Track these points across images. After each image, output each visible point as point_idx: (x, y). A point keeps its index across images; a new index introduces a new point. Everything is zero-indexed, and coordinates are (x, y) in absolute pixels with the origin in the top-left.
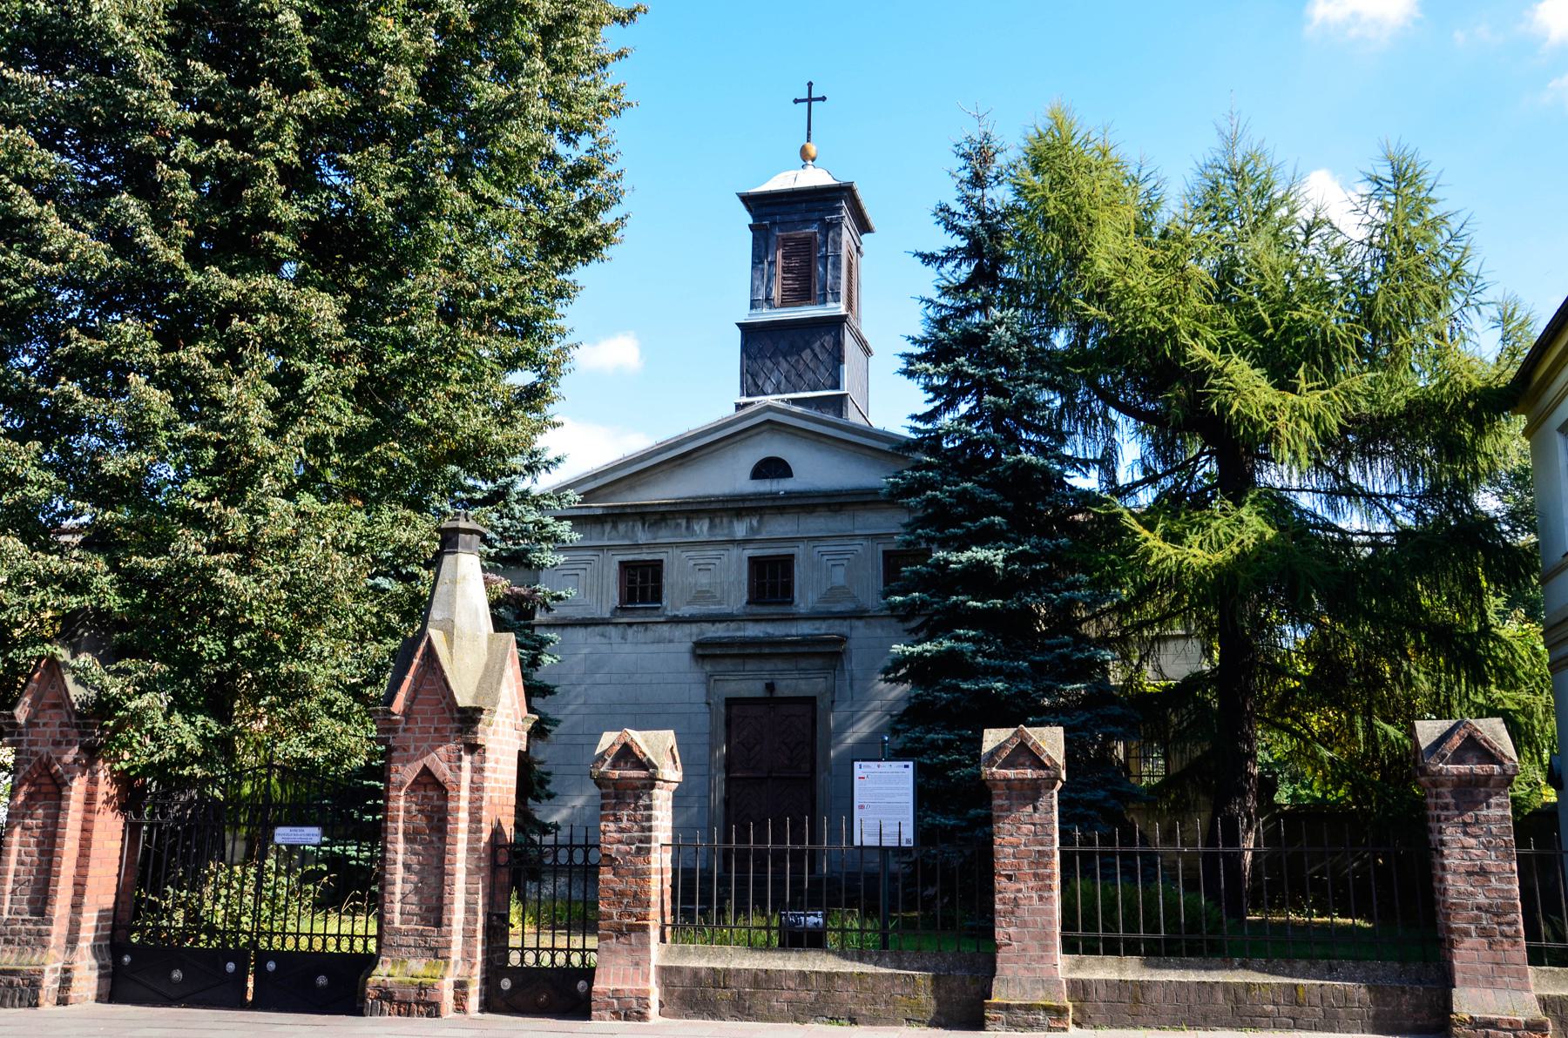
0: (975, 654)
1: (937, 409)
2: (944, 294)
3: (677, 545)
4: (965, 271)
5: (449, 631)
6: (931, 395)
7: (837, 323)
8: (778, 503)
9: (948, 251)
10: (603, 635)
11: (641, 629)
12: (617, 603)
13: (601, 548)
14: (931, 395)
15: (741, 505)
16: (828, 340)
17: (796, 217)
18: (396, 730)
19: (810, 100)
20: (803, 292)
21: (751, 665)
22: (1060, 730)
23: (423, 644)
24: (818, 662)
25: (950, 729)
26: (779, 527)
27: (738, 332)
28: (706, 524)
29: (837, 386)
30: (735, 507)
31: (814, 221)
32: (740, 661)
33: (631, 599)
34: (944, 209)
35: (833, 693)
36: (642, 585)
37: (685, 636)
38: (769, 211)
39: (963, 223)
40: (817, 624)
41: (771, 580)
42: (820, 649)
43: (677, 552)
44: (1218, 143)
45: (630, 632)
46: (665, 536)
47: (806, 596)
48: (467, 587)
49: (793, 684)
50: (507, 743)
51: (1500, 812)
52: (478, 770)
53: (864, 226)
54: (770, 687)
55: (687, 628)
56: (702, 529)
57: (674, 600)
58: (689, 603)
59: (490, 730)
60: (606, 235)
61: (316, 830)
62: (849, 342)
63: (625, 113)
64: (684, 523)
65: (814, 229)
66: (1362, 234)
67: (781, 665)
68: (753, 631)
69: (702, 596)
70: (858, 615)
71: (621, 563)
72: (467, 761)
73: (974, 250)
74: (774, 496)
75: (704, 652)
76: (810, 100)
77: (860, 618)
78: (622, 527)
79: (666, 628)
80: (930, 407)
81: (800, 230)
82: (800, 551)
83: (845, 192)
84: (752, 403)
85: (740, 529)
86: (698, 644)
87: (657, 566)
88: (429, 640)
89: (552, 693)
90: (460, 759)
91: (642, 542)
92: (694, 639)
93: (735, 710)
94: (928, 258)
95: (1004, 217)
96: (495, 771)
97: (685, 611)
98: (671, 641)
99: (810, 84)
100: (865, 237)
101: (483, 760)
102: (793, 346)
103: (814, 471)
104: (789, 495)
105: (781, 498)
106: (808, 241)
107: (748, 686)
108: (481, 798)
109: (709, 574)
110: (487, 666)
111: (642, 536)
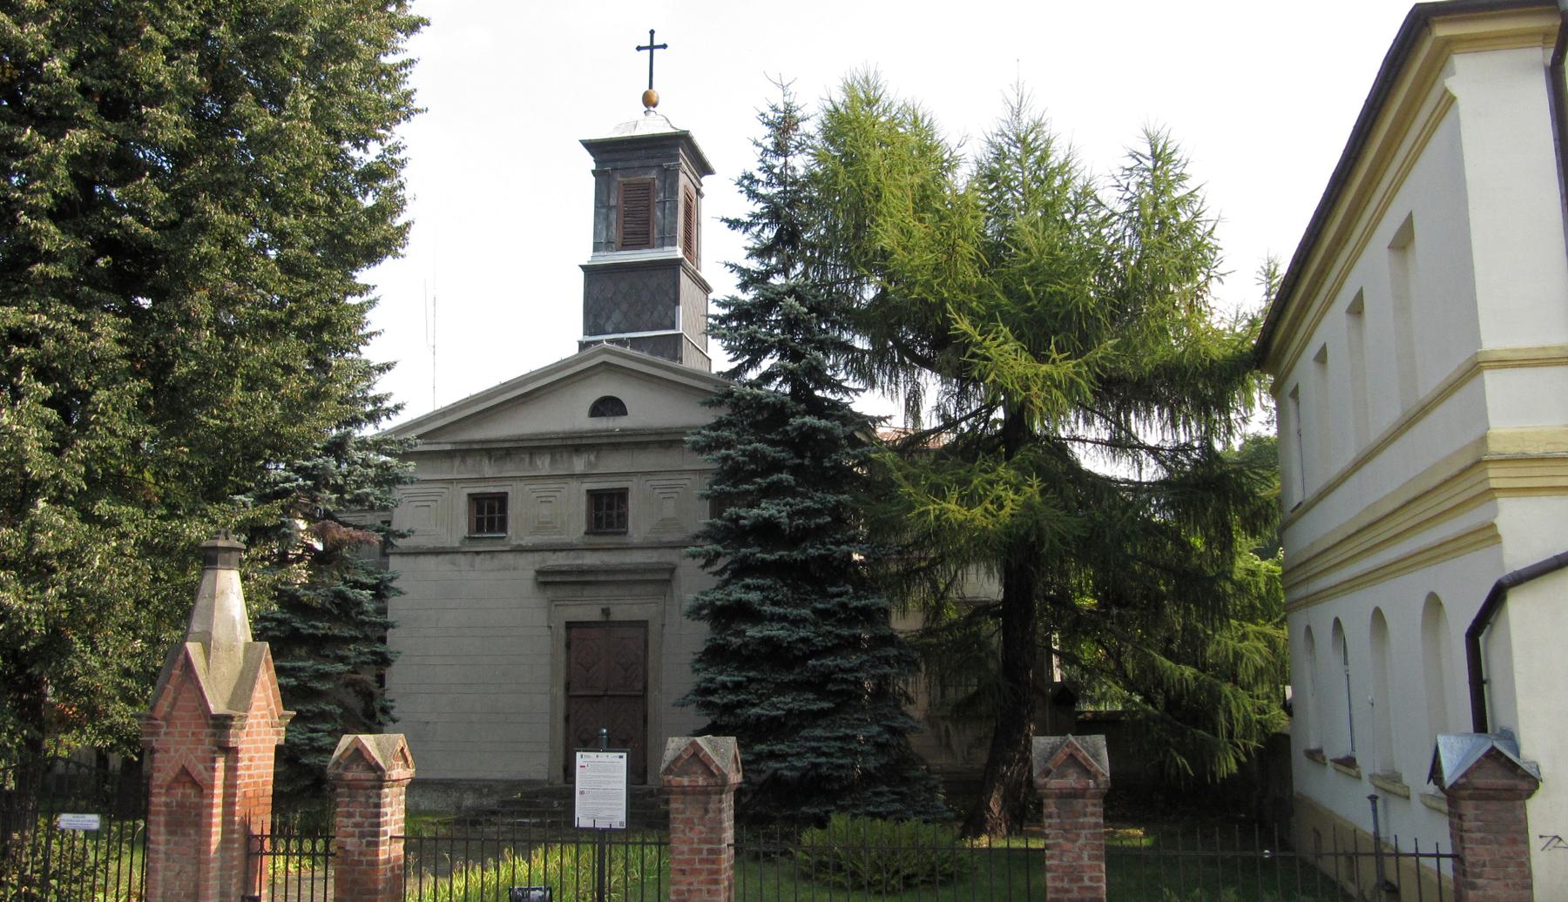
0: (762, 603)
1: (741, 366)
2: (750, 255)
4: (769, 234)
5: (207, 642)
6: (732, 356)
7: (675, 264)
8: (613, 440)
9: (754, 216)
11: (488, 557)
12: (465, 531)
13: (450, 481)
14: (732, 356)
17: (636, 164)
18: (158, 734)
19: (652, 47)
20: (638, 236)
22: (734, 739)
23: (181, 657)
25: (740, 669)
26: (615, 463)
27: (581, 274)
28: (547, 460)
29: (673, 327)
30: (575, 444)
31: (652, 167)
33: (479, 529)
34: (750, 178)
36: (489, 513)
37: (527, 566)
38: (610, 155)
39: (762, 190)
40: (650, 553)
41: (607, 510)
42: (650, 577)
43: (521, 485)
44: (1007, 115)
45: (478, 559)
46: (510, 469)
47: (640, 524)
48: (230, 599)
50: (263, 741)
51: (1092, 820)
52: (231, 770)
53: (704, 168)
54: (606, 612)
55: (530, 557)
56: (544, 465)
57: (517, 531)
59: (243, 735)
60: (402, 231)
61: (95, 817)
62: (685, 281)
63: (415, 118)
65: (653, 174)
66: (1122, 208)
68: (590, 560)
72: (220, 764)
73: (774, 213)
74: (609, 433)
75: (547, 580)
76: (652, 47)
78: (470, 462)
80: (735, 365)
82: (635, 487)
83: (682, 140)
84: (595, 343)
85: (579, 464)
86: (539, 572)
88: (187, 654)
90: (214, 760)
91: (488, 476)
93: (574, 632)
94: (734, 224)
95: (804, 185)
96: (249, 768)
97: (528, 541)
99: (652, 32)
100: (705, 180)
101: (237, 760)
102: (630, 292)
103: (647, 410)
104: (624, 432)
106: (647, 188)
107: (586, 610)
108: (235, 795)
109: (550, 508)
110: (242, 673)
111: (489, 470)
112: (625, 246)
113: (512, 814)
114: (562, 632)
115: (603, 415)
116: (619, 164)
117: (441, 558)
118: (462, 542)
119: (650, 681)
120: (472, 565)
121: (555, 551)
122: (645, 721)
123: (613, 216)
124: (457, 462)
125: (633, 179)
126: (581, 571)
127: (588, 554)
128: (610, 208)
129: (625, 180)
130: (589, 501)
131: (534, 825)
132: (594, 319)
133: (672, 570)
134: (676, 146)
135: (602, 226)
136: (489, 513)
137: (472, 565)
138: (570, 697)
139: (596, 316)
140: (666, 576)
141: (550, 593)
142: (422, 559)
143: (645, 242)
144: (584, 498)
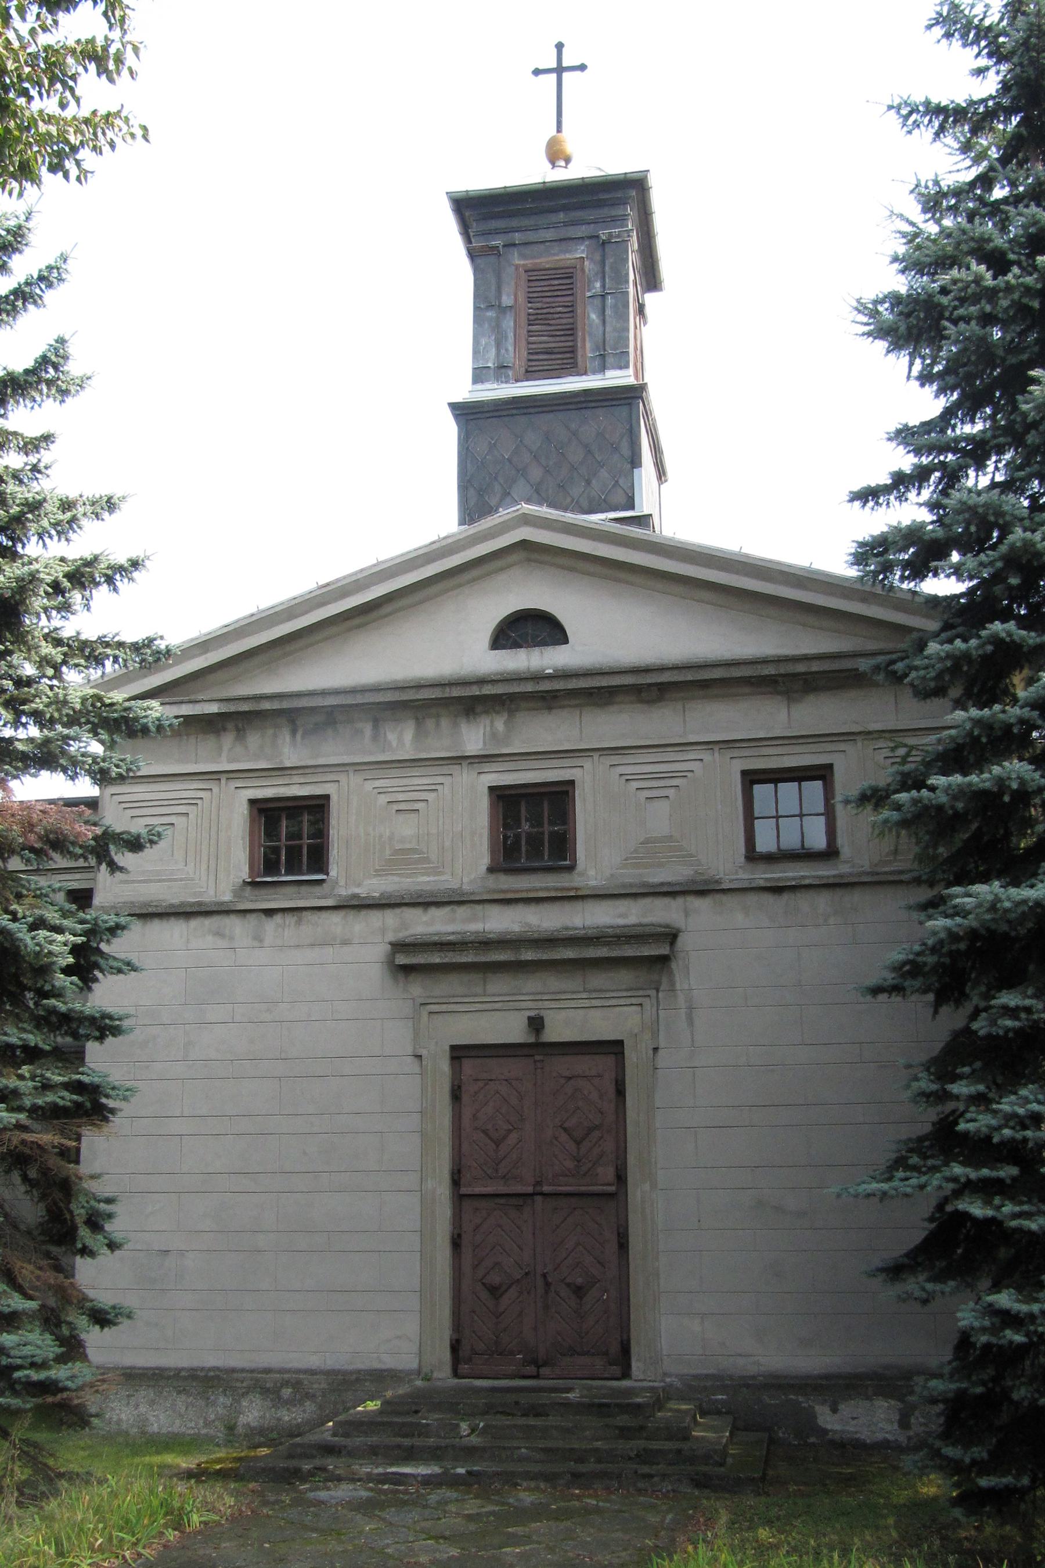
3: (357, 767)
10: (219, 934)
12: (244, 874)
13: (214, 776)
15: (475, 691)
16: (624, 411)
17: (549, 235)
19: (560, 70)
21: (499, 985)
24: (625, 977)
29: (631, 505)
32: (475, 977)
35: (655, 1034)
36: (291, 838)
37: (371, 938)
40: (623, 905)
41: (533, 826)
45: (270, 925)
46: (332, 751)
49: (578, 1015)
54: (536, 1024)
55: (376, 918)
57: (350, 869)
58: (378, 873)
64: (368, 729)
65: (581, 251)
67: (553, 982)
69: (403, 858)
70: (703, 889)
71: (252, 802)
75: (410, 962)
76: (560, 70)
77: (701, 893)
78: (254, 739)
79: (336, 918)
81: (558, 251)
85: (473, 737)
86: (399, 947)
87: (317, 808)
89: (116, 1031)
92: (391, 937)
93: (469, 1067)
97: (372, 887)
98: (345, 942)
99: (560, 46)
103: (605, 631)
105: (549, 677)
106: (566, 279)
109: (415, 825)
111: (291, 753)
112: (530, 374)
113: (373, 1452)
114: (445, 1066)
115: (516, 645)
116: (517, 237)
117: (194, 923)
118: (238, 893)
119: (631, 1160)
120: (259, 938)
121: (426, 905)
122: (623, 1245)
123: (508, 323)
124: (228, 739)
125: (546, 260)
126: (486, 943)
127: (495, 910)
128: (503, 310)
129: (529, 263)
130: (493, 806)
131: (427, 1481)
132: (477, 493)
133: (671, 936)
134: (623, 202)
135: (488, 340)
136: (291, 838)
137: (259, 938)
138: (460, 1199)
139: (481, 492)
140: (664, 950)
141: (417, 989)
142: (156, 925)
143: (568, 362)
144: (484, 803)
